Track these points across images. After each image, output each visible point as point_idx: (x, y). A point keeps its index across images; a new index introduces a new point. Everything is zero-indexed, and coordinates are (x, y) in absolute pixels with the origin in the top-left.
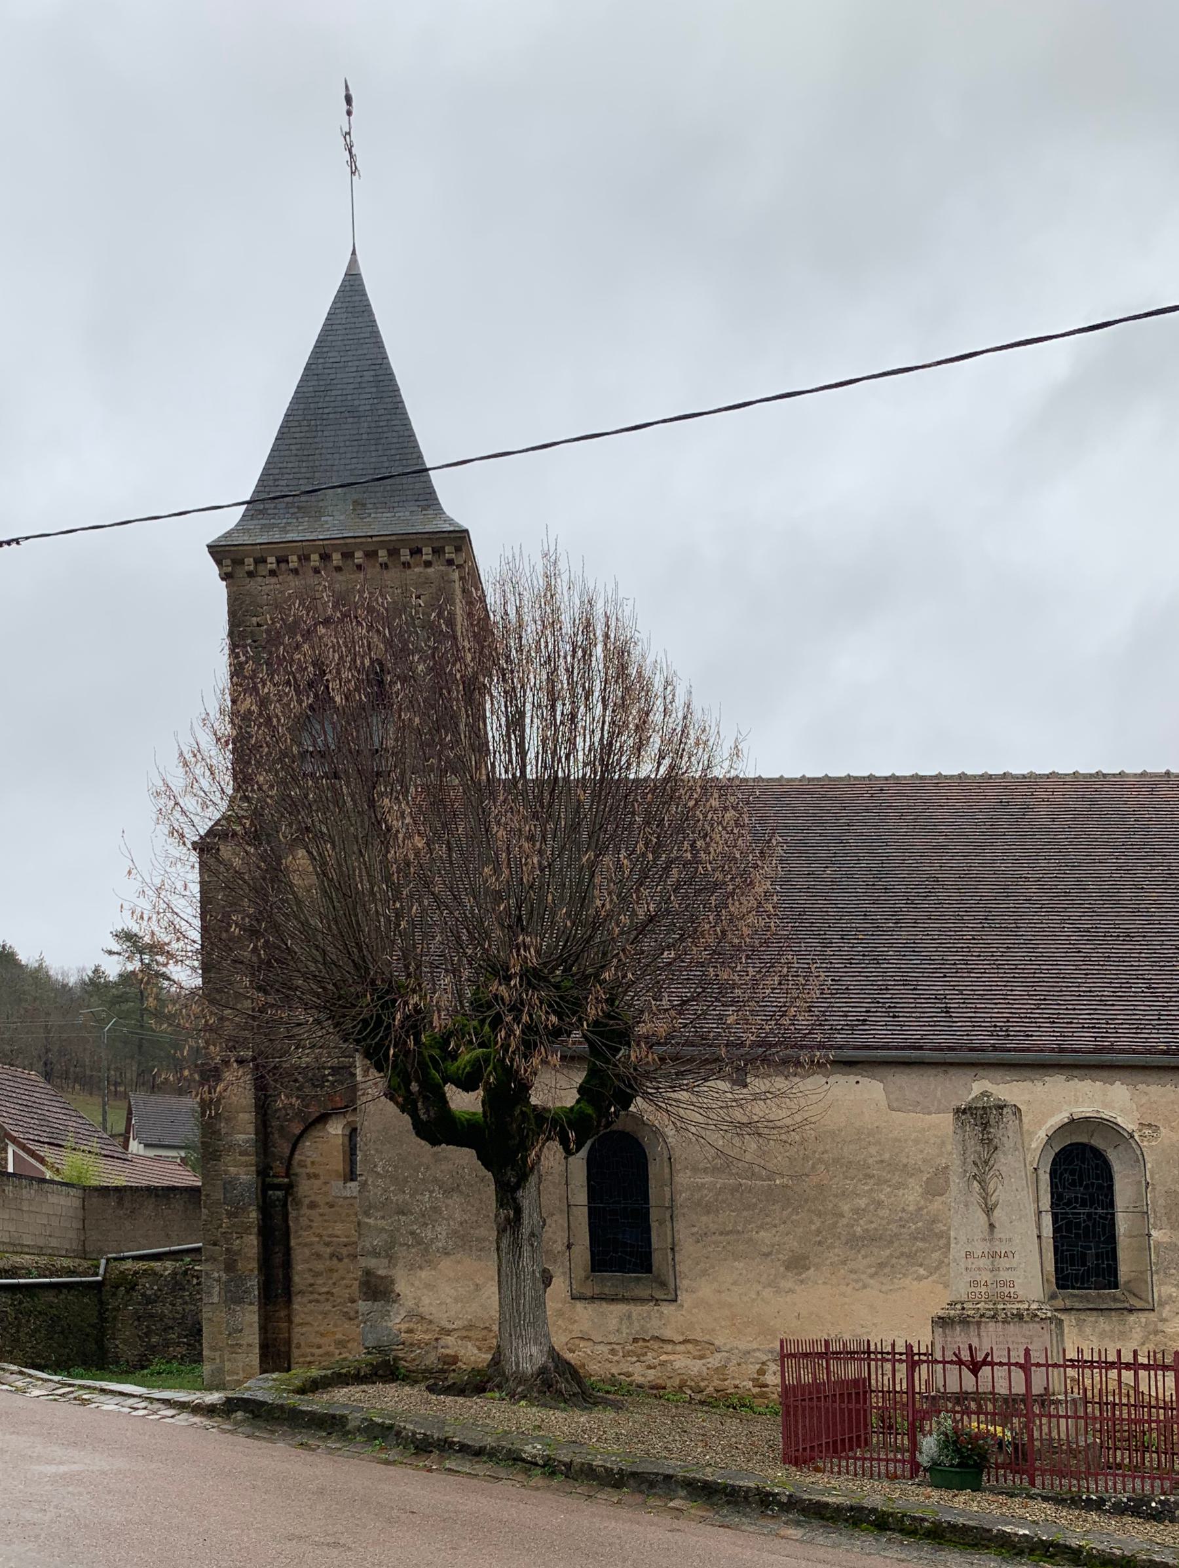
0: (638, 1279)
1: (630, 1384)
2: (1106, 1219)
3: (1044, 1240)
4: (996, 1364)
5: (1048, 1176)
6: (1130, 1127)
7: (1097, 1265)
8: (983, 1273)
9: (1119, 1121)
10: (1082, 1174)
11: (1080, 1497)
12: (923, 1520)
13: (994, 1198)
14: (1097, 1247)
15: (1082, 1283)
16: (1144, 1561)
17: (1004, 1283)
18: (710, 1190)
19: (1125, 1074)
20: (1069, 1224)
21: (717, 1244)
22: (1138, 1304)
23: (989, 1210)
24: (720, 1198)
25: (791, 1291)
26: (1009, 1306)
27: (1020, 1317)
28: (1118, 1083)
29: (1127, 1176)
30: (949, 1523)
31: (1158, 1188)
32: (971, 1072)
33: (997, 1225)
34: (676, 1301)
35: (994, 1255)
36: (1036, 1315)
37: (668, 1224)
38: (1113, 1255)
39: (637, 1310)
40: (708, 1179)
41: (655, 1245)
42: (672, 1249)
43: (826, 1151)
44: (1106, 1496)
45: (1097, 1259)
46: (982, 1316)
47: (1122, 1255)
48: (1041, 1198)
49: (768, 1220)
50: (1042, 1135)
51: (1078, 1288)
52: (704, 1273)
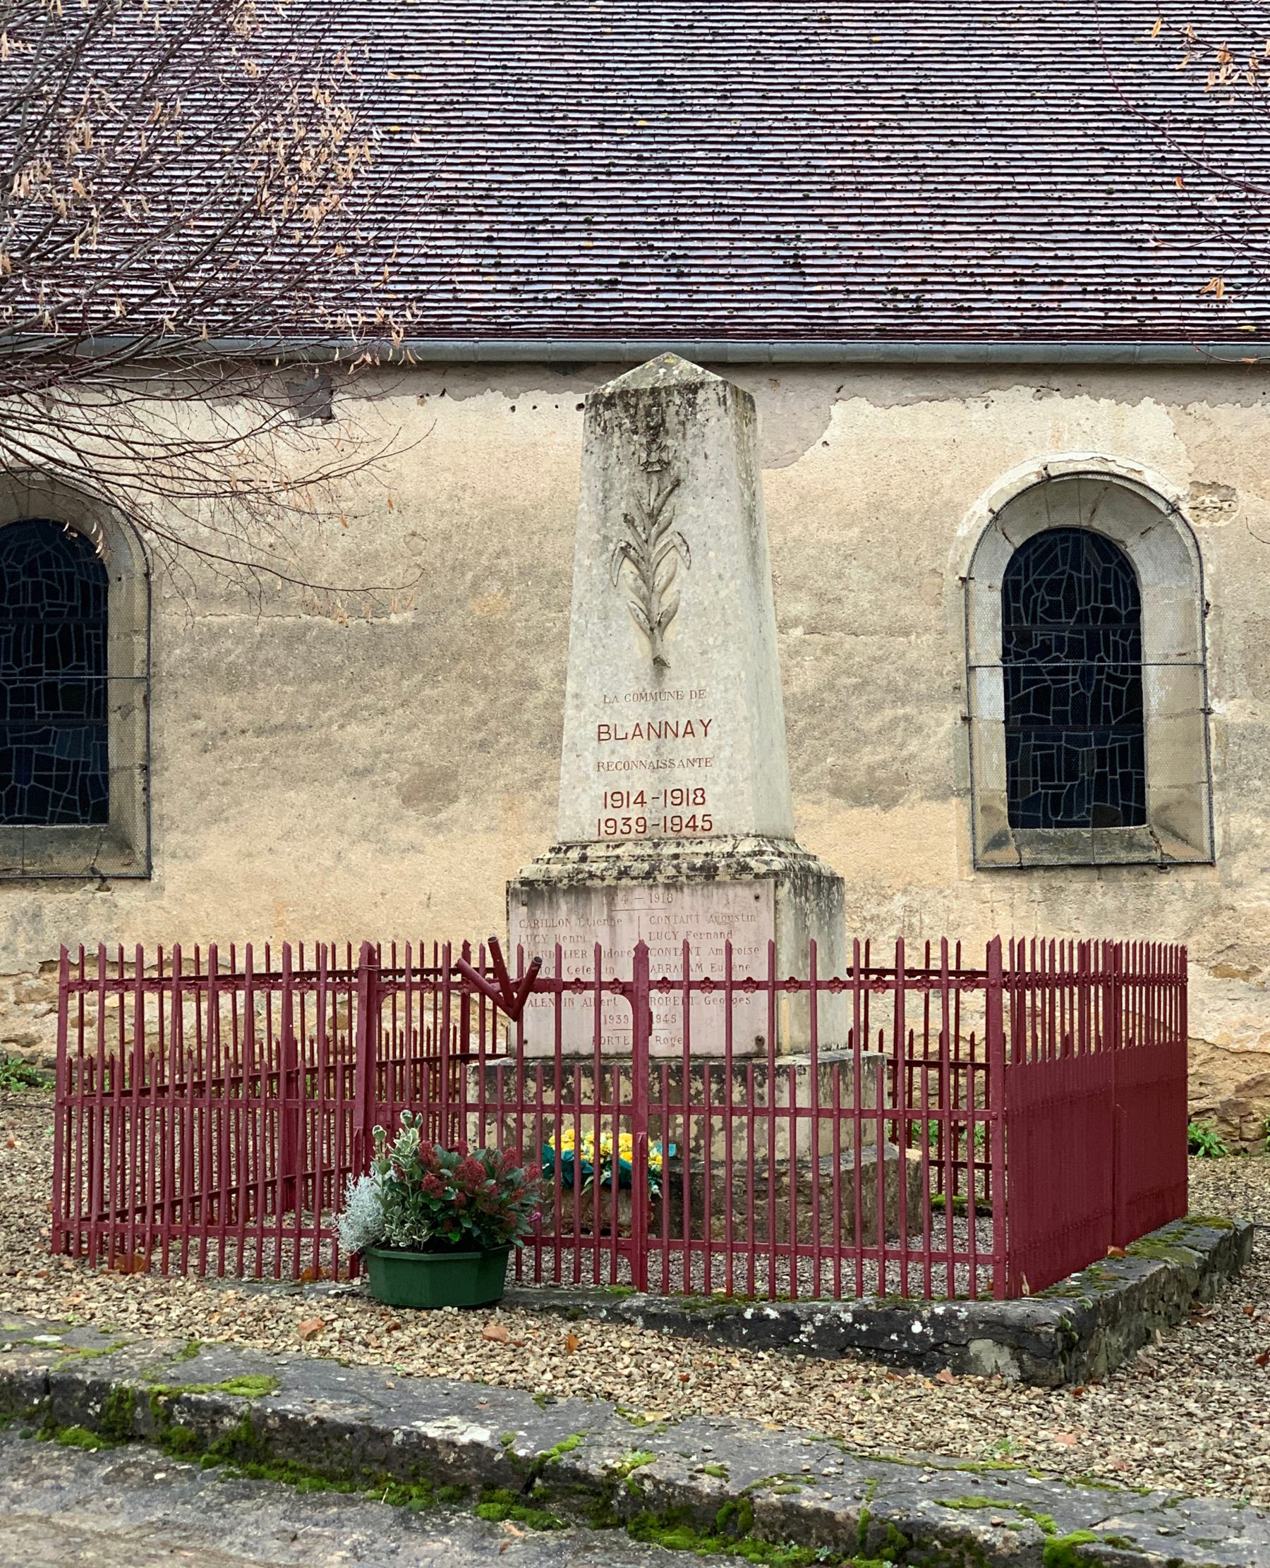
0: (78, 833)
1: (30, 1061)
2: (1122, 682)
3: (979, 726)
4: (567, 986)
5: (997, 597)
6: (1171, 491)
7: (1101, 777)
8: (636, 773)
9: (1149, 478)
10: (1071, 596)
11: (740, 1314)
12: (220, 1410)
13: (667, 600)
14: (1101, 740)
15: (1069, 813)
16: (771, 1509)
17: (680, 796)
18: (239, 640)
19: (1165, 384)
20: (1042, 699)
21: (247, 753)
22: (1178, 852)
23: (655, 626)
24: (262, 656)
25: (413, 848)
26: (689, 849)
27: (708, 872)
28: (1148, 401)
29: (1166, 593)
30: (283, 1417)
31: (1228, 614)
32: (828, 383)
33: (671, 660)
34: (147, 877)
35: (662, 731)
36: (745, 868)
37: (139, 716)
38: (1135, 754)
39: (52, 901)
40: (234, 617)
41: (113, 762)
42: (145, 768)
43: (504, 552)
44: (800, 1308)
45: (1101, 765)
46: (623, 873)
47: (1155, 754)
48: (976, 637)
49: (368, 699)
50: (979, 510)
51: (1059, 825)
52: (217, 817)
